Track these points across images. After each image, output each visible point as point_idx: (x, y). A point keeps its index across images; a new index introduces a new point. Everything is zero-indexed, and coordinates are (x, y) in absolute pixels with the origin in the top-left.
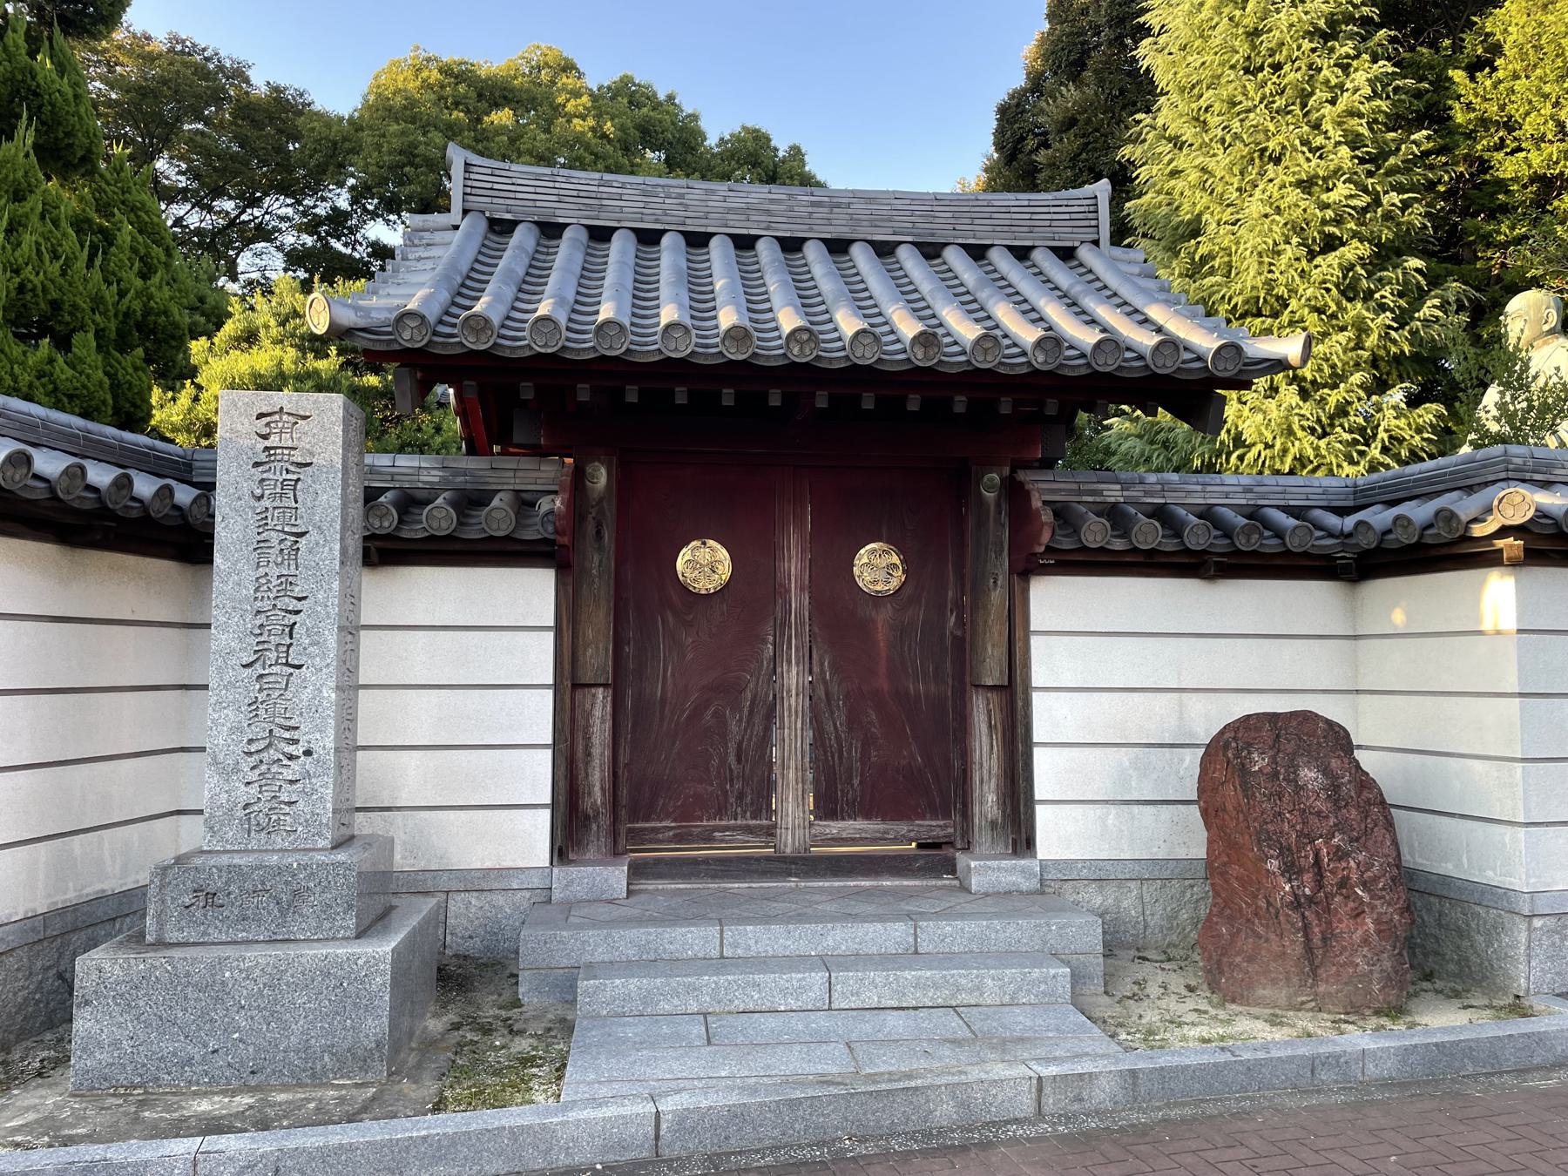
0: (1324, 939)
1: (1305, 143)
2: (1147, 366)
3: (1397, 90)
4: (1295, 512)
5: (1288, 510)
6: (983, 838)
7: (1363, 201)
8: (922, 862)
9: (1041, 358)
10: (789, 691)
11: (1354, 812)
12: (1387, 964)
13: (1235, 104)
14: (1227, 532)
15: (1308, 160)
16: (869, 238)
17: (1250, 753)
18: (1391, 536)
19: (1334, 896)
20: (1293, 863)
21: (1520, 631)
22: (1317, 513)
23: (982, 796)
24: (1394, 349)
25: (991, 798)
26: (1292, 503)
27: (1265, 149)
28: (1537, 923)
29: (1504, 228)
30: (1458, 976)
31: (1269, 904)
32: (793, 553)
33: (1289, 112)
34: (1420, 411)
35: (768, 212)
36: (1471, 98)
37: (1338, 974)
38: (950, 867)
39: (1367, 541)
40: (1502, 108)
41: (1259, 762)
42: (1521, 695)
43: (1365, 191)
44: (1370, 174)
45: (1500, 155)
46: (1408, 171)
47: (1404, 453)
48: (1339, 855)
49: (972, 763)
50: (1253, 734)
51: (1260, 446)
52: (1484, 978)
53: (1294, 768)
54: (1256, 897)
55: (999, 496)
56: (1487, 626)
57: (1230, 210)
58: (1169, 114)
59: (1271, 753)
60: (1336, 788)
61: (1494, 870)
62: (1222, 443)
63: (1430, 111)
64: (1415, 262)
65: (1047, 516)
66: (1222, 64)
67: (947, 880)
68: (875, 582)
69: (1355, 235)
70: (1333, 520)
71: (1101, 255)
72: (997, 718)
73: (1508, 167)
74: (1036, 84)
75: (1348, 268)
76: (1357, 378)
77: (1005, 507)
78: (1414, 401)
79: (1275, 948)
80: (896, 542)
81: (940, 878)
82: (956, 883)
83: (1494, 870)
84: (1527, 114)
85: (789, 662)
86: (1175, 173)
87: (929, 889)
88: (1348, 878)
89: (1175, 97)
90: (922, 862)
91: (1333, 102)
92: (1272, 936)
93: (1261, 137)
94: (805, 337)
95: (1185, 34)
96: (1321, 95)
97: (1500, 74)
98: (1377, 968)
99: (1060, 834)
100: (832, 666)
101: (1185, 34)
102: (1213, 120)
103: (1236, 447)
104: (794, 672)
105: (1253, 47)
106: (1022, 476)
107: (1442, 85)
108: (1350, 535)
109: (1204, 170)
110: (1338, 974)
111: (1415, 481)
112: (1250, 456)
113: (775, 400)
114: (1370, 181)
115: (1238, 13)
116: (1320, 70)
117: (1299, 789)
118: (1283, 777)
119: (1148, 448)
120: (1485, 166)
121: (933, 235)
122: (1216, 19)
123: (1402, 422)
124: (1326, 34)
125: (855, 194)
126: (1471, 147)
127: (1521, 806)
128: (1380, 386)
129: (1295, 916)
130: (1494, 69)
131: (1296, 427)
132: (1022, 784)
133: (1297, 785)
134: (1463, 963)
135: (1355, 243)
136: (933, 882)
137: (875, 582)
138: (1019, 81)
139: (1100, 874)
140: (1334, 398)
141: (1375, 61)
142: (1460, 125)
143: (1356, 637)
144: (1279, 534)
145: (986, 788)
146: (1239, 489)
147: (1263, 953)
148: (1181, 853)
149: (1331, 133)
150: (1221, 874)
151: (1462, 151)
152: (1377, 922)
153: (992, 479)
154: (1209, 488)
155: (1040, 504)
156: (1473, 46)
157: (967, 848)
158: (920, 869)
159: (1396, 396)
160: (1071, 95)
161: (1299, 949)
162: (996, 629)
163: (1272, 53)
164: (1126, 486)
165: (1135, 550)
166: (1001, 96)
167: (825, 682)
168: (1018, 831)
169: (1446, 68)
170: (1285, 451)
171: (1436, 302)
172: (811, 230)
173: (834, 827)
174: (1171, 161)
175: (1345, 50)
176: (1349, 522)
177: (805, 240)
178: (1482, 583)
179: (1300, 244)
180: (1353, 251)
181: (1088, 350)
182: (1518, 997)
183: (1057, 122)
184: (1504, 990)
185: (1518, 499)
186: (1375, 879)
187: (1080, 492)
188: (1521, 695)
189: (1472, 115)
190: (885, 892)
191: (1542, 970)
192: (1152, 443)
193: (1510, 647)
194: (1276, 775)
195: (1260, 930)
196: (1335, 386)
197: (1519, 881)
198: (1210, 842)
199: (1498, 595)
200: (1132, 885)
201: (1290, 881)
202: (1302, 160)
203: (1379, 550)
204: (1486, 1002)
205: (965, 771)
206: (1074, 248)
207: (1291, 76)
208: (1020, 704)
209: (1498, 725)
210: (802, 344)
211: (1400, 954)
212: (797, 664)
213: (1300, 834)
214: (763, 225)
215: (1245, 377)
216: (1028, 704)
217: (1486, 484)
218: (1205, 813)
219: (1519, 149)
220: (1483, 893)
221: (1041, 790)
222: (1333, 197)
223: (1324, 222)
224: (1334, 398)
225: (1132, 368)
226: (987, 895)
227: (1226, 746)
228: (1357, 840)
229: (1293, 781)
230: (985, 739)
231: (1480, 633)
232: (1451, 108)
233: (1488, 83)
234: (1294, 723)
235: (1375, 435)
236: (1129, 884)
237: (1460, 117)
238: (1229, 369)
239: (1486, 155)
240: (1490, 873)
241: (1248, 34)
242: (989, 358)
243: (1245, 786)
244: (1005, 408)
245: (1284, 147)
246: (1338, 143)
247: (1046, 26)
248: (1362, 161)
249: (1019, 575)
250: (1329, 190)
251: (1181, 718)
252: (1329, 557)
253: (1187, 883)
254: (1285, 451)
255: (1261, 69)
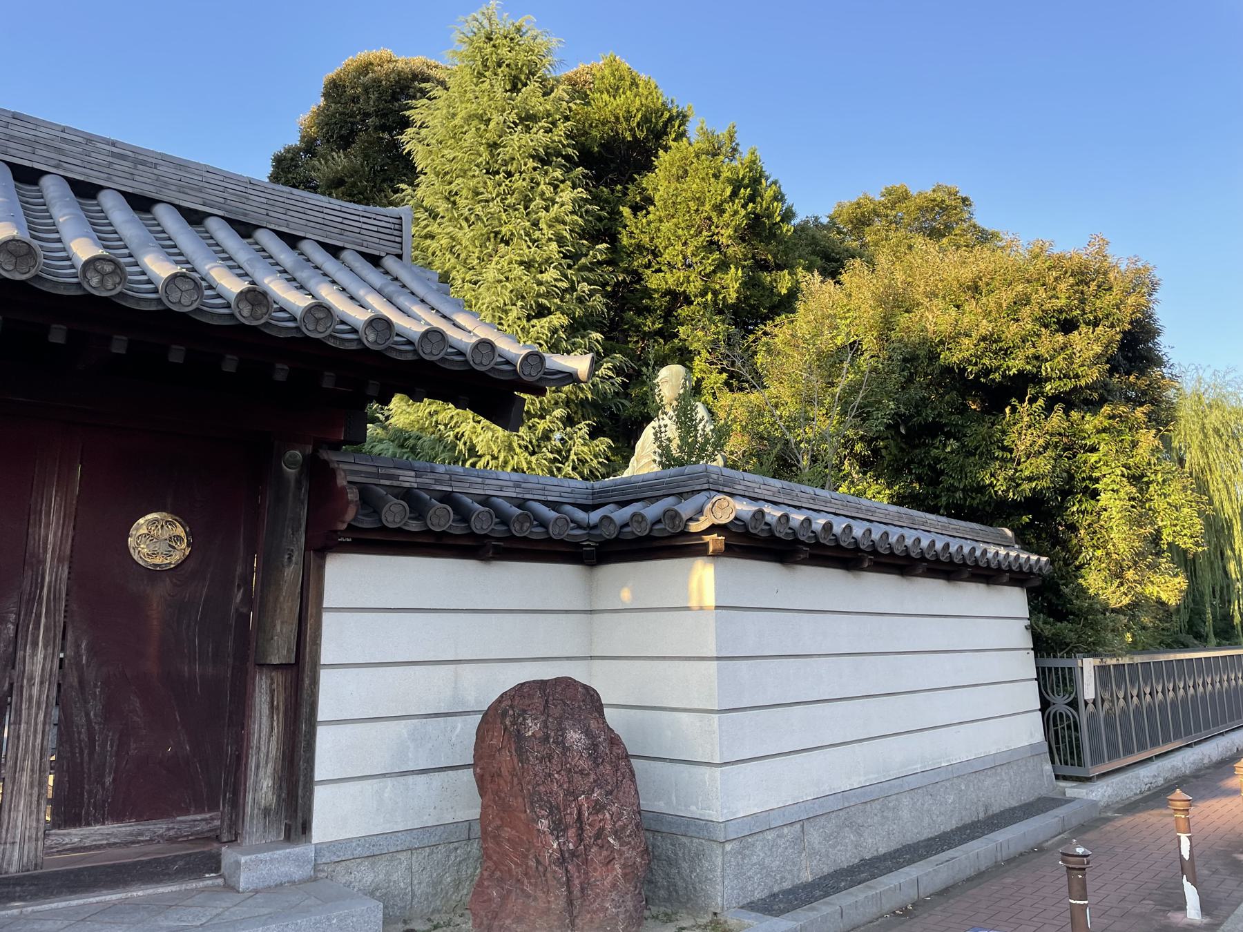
0: (582, 890)
1: (528, 234)
2: (466, 362)
3: (587, 211)
4: (554, 506)
5: (546, 503)
6: (253, 826)
7: (565, 285)
8: (181, 863)
9: (372, 337)
10: (31, 678)
11: (608, 767)
12: (630, 904)
13: (478, 194)
14: (504, 519)
15: (529, 247)
16: (177, 202)
17: (524, 719)
18: (626, 530)
19: (591, 847)
20: (560, 820)
21: (717, 607)
22: (568, 508)
23: (256, 782)
24: (581, 395)
25: (267, 783)
26: (550, 499)
27: (497, 233)
28: (728, 847)
29: (649, 323)
30: (668, 900)
31: (538, 862)
32: (53, 518)
33: (516, 210)
34: (597, 442)
35: (59, 150)
36: (633, 229)
37: (592, 921)
38: (213, 864)
39: (609, 533)
40: (652, 239)
41: (532, 727)
42: (718, 658)
43: (566, 278)
44: (570, 267)
45: (649, 272)
46: (591, 270)
47: (586, 471)
48: (598, 808)
49: (248, 747)
50: (527, 702)
51: (488, 457)
52: (689, 899)
53: (561, 730)
54: (526, 857)
55: (301, 473)
56: (693, 603)
57: (471, 272)
58: (427, 190)
59: (543, 718)
60: (595, 746)
61: (697, 805)
62: (460, 451)
63: (603, 230)
64: (598, 336)
65: (353, 495)
66: (470, 162)
67: (210, 880)
68: (154, 555)
69: (559, 308)
70: (580, 515)
71: (405, 266)
72: (280, 700)
73: (653, 281)
74: (309, 147)
75: (554, 331)
76: (559, 412)
77: (305, 484)
78: (593, 434)
79: (542, 905)
80: (181, 512)
81: (200, 877)
82: (220, 881)
83: (697, 805)
84: (666, 248)
85: (35, 644)
86: (431, 236)
87: (188, 894)
88: (603, 829)
89: (432, 177)
90: (181, 863)
91: (547, 209)
92: (540, 894)
93: (496, 222)
94: (109, 268)
95: (441, 132)
96: (538, 202)
97: (651, 217)
98: (622, 910)
99: (336, 813)
100: (90, 649)
101: (441, 132)
102: (461, 202)
103: (470, 457)
104: (40, 655)
105: (492, 156)
106: (326, 455)
107: (615, 215)
108: (595, 527)
109: (453, 238)
110: (592, 921)
111: (640, 487)
112: (480, 464)
113: (57, 335)
114: (569, 271)
115: (483, 127)
116: (538, 184)
117: (566, 749)
118: (553, 739)
119: (398, 451)
120: (638, 277)
121: (245, 215)
122: (466, 128)
123: (586, 449)
124: (544, 160)
125: (164, 158)
126: (630, 263)
127: (717, 749)
128: (569, 421)
129: (560, 872)
130: (648, 213)
131: (515, 445)
132: (302, 765)
133: (564, 747)
134: (672, 888)
135: (558, 314)
136: (193, 885)
137: (154, 555)
138: (295, 141)
139: (372, 850)
140: (542, 425)
141: (574, 187)
142: (625, 247)
143: (591, 612)
144: (543, 524)
145: (261, 773)
146: (511, 484)
147: (531, 912)
148: (448, 818)
149: (545, 231)
150: (494, 837)
151: (624, 265)
152: (624, 866)
153: (296, 456)
154: (488, 481)
155: (345, 483)
156: (634, 195)
157: (234, 840)
158: (178, 872)
159: (583, 429)
160: (340, 161)
161: (562, 903)
162: (286, 606)
163: (505, 163)
164: (419, 473)
165: (429, 532)
166: (278, 148)
167: (78, 664)
168: (294, 815)
169: (616, 205)
170: (506, 462)
171: (610, 365)
172: (109, 180)
173: (75, 835)
174: (427, 226)
175: (555, 174)
176: (595, 516)
177: (102, 188)
178: (690, 569)
179: (522, 307)
180: (558, 319)
181: (416, 338)
182: (715, 914)
183: (328, 179)
184: (704, 909)
185: (725, 504)
186: (624, 828)
187: (379, 476)
188: (718, 658)
189: (633, 241)
190: (136, 905)
191: (732, 888)
192: (402, 446)
193: (711, 619)
194: (547, 737)
195: (529, 889)
196: (542, 417)
197: (716, 813)
198: (484, 807)
199: (702, 579)
200: (403, 856)
201: (557, 838)
202: (525, 247)
203: (617, 540)
204: (692, 922)
205: (239, 758)
206: (380, 258)
207: (519, 183)
208: (307, 682)
209: (700, 684)
210: (103, 275)
211: (640, 893)
212: (45, 647)
213: (568, 793)
214: (53, 163)
215: (541, 384)
216: (315, 682)
217: (693, 493)
218: (480, 780)
219: (660, 270)
220: (688, 826)
221: (321, 770)
222: (545, 277)
223: (539, 295)
224: (542, 425)
225: (453, 361)
226: (256, 892)
227: (504, 714)
228: (611, 793)
229: (561, 743)
230: (265, 720)
231: (688, 608)
232: (620, 233)
233: (644, 221)
234: (559, 689)
235: (568, 457)
236: (400, 856)
237: (625, 241)
238: (531, 375)
239: (641, 270)
240: (693, 808)
241: (489, 145)
242: (320, 329)
243: (520, 751)
244: (328, 382)
245: (512, 234)
246: (550, 240)
247: (322, 102)
248: (565, 257)
249: (316, 551)
250: (541, 272)
251: (455, 688)
252: (578, 545)
253: (452, 846)
254: (506, 462)
255: (497, 173)
